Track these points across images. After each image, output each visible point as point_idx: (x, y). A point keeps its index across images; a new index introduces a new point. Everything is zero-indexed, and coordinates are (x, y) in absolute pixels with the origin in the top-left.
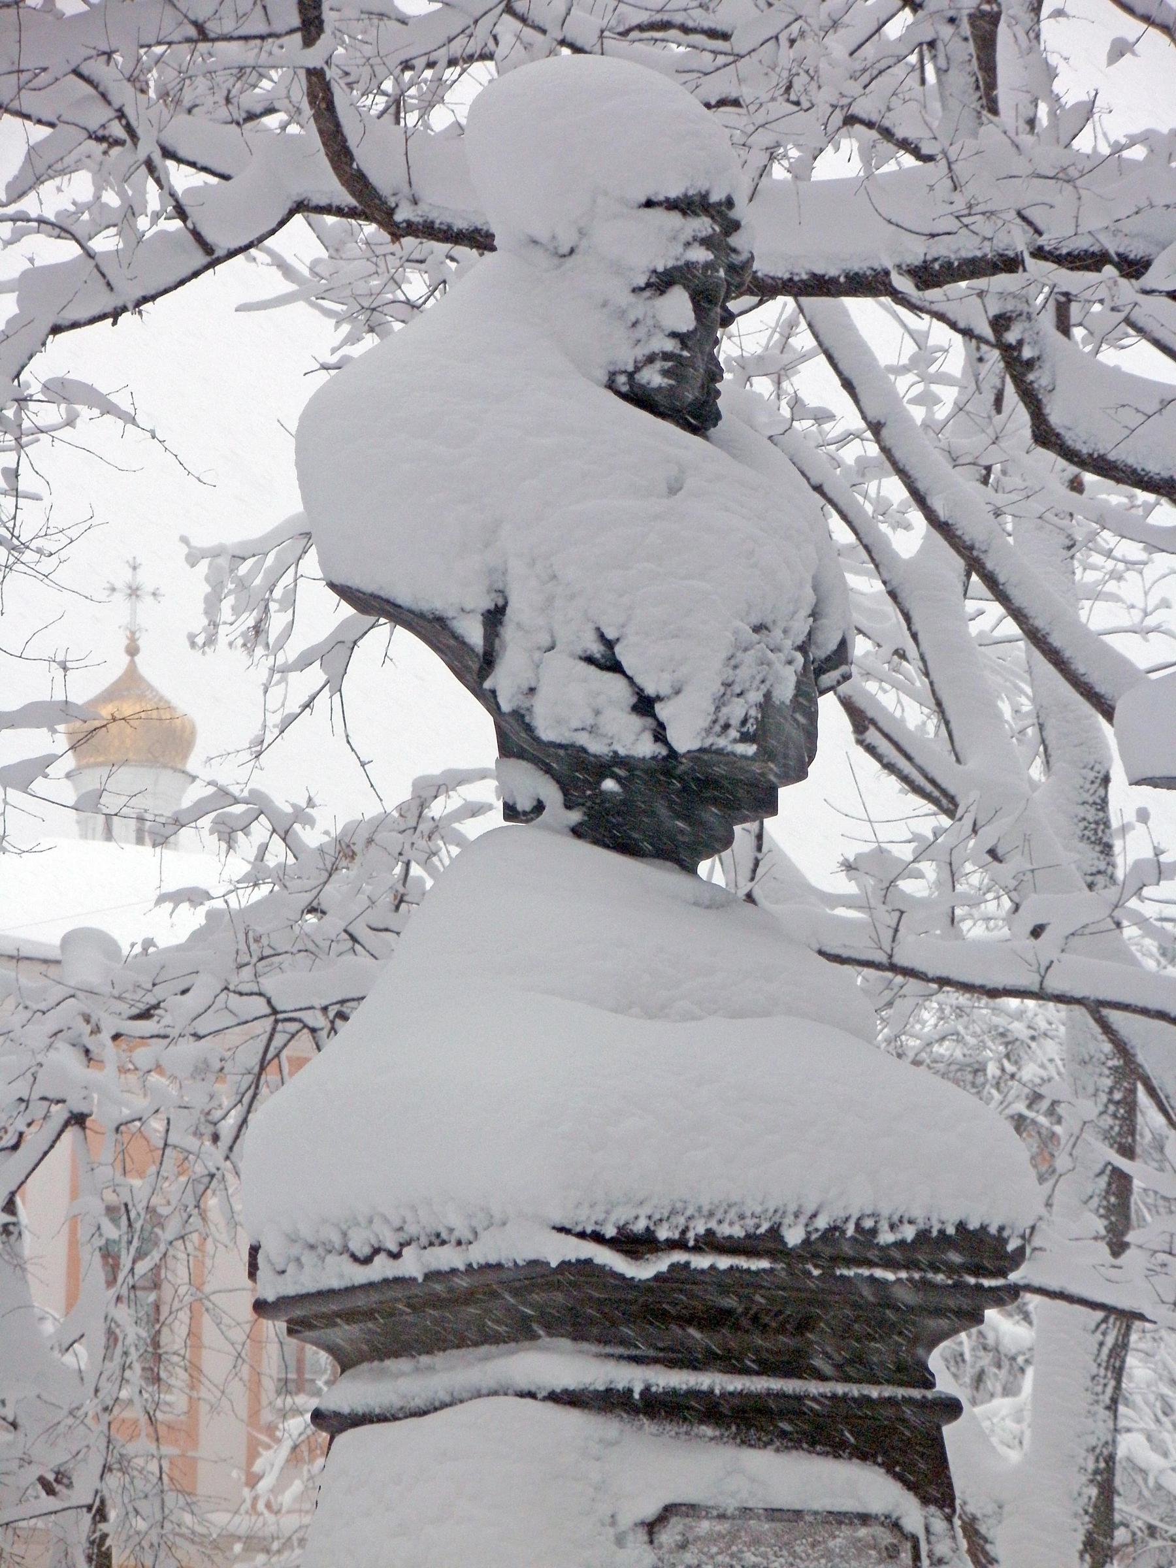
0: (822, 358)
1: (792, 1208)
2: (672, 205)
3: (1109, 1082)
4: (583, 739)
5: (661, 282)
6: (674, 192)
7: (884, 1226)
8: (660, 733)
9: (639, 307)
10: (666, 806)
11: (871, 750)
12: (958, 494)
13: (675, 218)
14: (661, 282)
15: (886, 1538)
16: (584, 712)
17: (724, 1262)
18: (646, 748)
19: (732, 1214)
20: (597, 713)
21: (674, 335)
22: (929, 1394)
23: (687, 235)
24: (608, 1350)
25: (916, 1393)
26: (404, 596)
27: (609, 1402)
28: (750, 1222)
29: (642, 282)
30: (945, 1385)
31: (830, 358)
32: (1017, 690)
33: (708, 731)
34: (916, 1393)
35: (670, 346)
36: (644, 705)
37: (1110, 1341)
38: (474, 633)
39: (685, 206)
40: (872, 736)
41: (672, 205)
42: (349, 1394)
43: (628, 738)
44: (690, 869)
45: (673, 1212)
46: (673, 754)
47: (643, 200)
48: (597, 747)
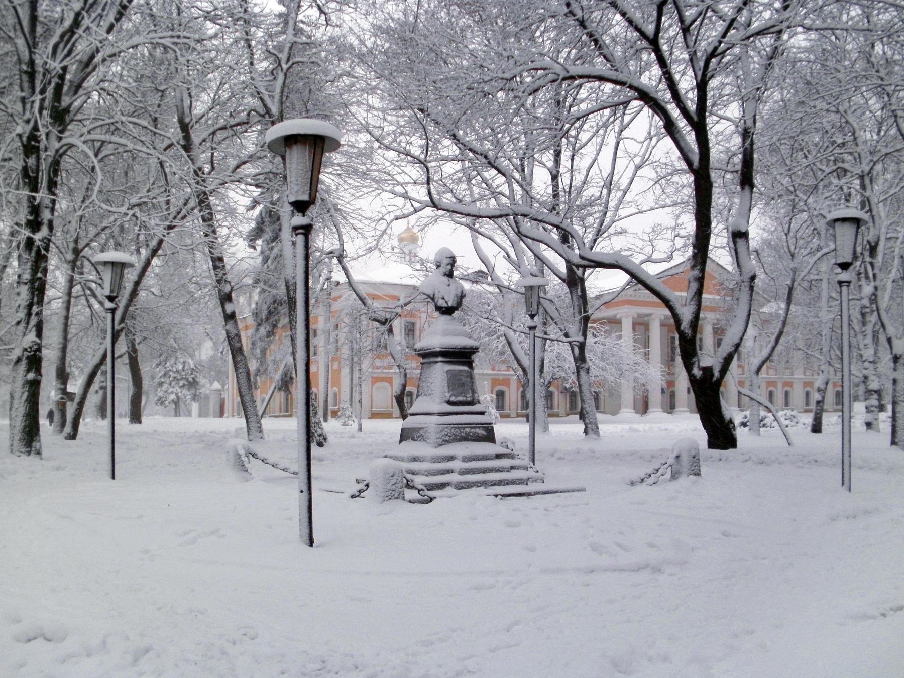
16: (441, 303)
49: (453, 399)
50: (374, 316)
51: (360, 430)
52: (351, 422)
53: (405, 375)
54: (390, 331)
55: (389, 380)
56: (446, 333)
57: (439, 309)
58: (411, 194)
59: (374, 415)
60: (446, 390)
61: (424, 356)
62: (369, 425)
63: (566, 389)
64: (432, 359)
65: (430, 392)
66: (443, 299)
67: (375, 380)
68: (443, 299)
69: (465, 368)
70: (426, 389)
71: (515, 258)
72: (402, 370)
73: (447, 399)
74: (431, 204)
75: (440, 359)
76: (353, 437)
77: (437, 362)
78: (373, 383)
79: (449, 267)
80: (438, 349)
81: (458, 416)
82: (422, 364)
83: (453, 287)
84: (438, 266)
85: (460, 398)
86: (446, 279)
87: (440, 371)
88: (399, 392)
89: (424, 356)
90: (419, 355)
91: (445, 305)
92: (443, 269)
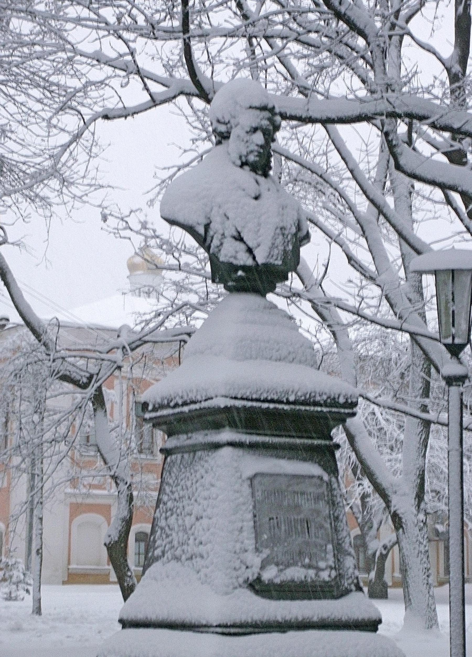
0: (336, 151)
1: (291, 390)
2: (256, 108)
3: (422, 362)
4: (232, 260)
5: (255, 130)
6: (257, 104)
7: (318, 395)
8: (254, 258)
9: (247, 137)
10: (254, 279)
11: (353, 266)
12: (376, 192)
13: (258, 112)
14: (255, 130)
15: (318, 482)
16: (231, 252)
17: (272, 406)
18: (250, 262)
19: (274, 392)
20: (237, 252)
21: (257, 145)
22: (331, 443)
23: (261, 116)
24: (248, 431)
25: (327, 442)
26: (181, 219)
27: (252, 446)
28: (279, 394)
29: (248, 130)
30: (336, 440)
31: (338, 151)
32: (393, 250)
33: (268, 257)
34: (327, 442)
35: (256, 148)
36: (250, 251)
37: (423, 437)
38: (201, 230)
39: (263, 108)
40: (352, 262)
41: (256, 108)
42: (172, 443)
43: (245, 258)
44: (264, 295)
45: (257, 391)
46: (257, 265)
47: (248, 106)
48: (235, 262)
49: (270, 574)
50: (64, 368)
51: (38, 610)
52: (22, 593)
53: (131, 498)
54: (99, 400)
55: (104, 510)
56: (249, 351)
57: (222, 272)
58: (143, 62)
59: (74, 578)
60: (250, 544)
61: (172, 426)
62: (57, 597)
63: (437, 533)
64: (199, 437)
65: (191, 548)
66: (239, 238)
67: (76, 509)
68: (239, 238)
69: (313, 469)
70: (176, 537)
71: (372, 268)
72: (123, 487)
73: (251, 575)
74: (193, 89)
75: (227, 435)
76: (18, 629)
77: (217, 446)
78: (73, 516)
79: (259, 138)
80: (222, 403)
81: (291, 634)
82: (167, 452)
83: (269, 201)
84: (223, 137)
85: (296, 573)
86: (246, 175)
87: (226, 477)
88: (115, 537)
89: (172, 426)
90: (157, 423)
91: (244, 259)
92: (235, 146)
